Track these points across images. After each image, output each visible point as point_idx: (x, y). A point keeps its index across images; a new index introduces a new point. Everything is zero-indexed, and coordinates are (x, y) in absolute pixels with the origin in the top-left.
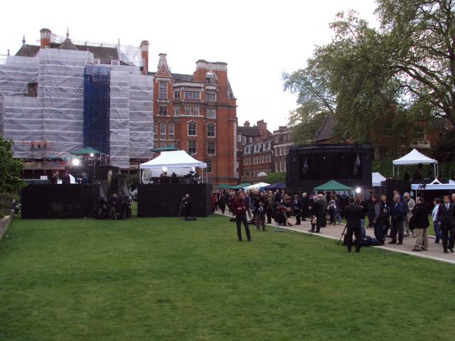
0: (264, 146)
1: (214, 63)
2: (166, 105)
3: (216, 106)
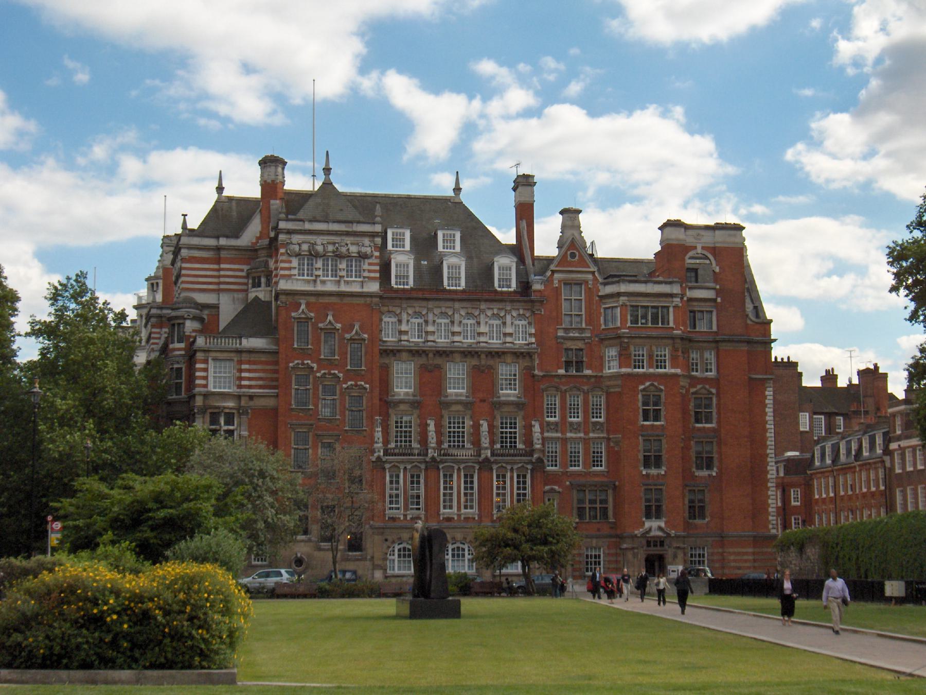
0: (865, 444)
1: (707, 228)
2: (580, 345)
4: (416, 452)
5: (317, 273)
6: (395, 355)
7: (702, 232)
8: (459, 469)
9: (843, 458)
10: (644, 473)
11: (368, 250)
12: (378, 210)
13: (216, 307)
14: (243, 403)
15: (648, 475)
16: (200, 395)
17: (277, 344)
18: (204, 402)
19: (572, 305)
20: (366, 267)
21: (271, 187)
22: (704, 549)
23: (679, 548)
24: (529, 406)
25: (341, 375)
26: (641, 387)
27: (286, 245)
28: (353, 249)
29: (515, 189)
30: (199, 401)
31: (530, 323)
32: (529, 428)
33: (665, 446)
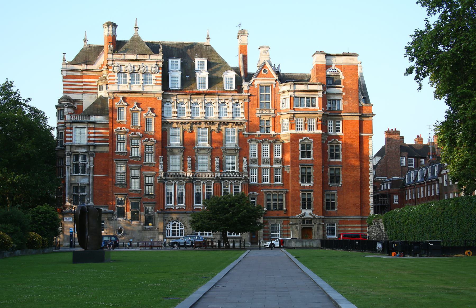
0: (430, 171)
8: (204, 183)
9: (419, 179)
10: (302, 185)
12: (161, 49)
13: (81, 101)
15: (303, 186)
16: (68, 145)
22: (334, 224)
26: (300, 140)
30: (68, 149)
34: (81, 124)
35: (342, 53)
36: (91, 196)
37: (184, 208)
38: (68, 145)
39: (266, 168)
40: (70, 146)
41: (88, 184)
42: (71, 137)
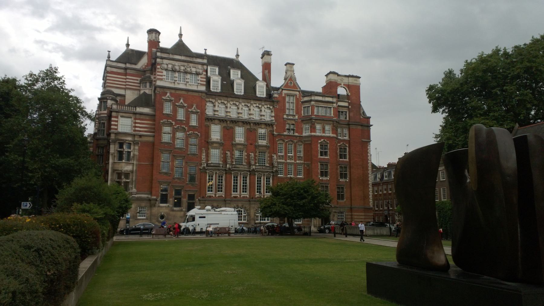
1: (346, 76)
3: (349, 125)
4: (221, 166)
5: (176, 79)
6: (212, 121)
7: (344, 78)
8: (241, 174)
11: (201, 71)
13: (124, 96)
14: (136, 139)
15: (322, 180)
16: (113, 133)
17: (155, 111)
18: (115, 137)
19: (290, 105)
20: (199, 78)
21: (154, 43)
23: (335, 212)
24: (272, 148)
25: (186, 128)
26: (320, 141)
27: (160, 64)
28: (194, 70)
29: (262, 58)
30: (113, 136)
31: (272, 112)
32: (271, 157)
33: (329, 167)
34: (127, 114)
35: (348, 74)
36: (134, 183)
37: (224, 196)
38: (113, 133)
39: (291, 164)
40: (115, 134)
41: (132, 172)
42: (117, 125)
